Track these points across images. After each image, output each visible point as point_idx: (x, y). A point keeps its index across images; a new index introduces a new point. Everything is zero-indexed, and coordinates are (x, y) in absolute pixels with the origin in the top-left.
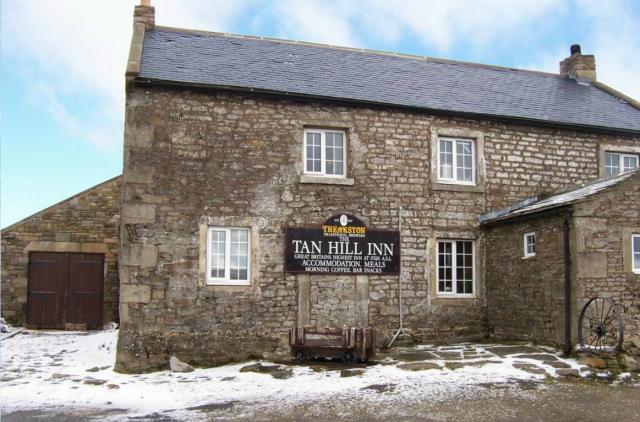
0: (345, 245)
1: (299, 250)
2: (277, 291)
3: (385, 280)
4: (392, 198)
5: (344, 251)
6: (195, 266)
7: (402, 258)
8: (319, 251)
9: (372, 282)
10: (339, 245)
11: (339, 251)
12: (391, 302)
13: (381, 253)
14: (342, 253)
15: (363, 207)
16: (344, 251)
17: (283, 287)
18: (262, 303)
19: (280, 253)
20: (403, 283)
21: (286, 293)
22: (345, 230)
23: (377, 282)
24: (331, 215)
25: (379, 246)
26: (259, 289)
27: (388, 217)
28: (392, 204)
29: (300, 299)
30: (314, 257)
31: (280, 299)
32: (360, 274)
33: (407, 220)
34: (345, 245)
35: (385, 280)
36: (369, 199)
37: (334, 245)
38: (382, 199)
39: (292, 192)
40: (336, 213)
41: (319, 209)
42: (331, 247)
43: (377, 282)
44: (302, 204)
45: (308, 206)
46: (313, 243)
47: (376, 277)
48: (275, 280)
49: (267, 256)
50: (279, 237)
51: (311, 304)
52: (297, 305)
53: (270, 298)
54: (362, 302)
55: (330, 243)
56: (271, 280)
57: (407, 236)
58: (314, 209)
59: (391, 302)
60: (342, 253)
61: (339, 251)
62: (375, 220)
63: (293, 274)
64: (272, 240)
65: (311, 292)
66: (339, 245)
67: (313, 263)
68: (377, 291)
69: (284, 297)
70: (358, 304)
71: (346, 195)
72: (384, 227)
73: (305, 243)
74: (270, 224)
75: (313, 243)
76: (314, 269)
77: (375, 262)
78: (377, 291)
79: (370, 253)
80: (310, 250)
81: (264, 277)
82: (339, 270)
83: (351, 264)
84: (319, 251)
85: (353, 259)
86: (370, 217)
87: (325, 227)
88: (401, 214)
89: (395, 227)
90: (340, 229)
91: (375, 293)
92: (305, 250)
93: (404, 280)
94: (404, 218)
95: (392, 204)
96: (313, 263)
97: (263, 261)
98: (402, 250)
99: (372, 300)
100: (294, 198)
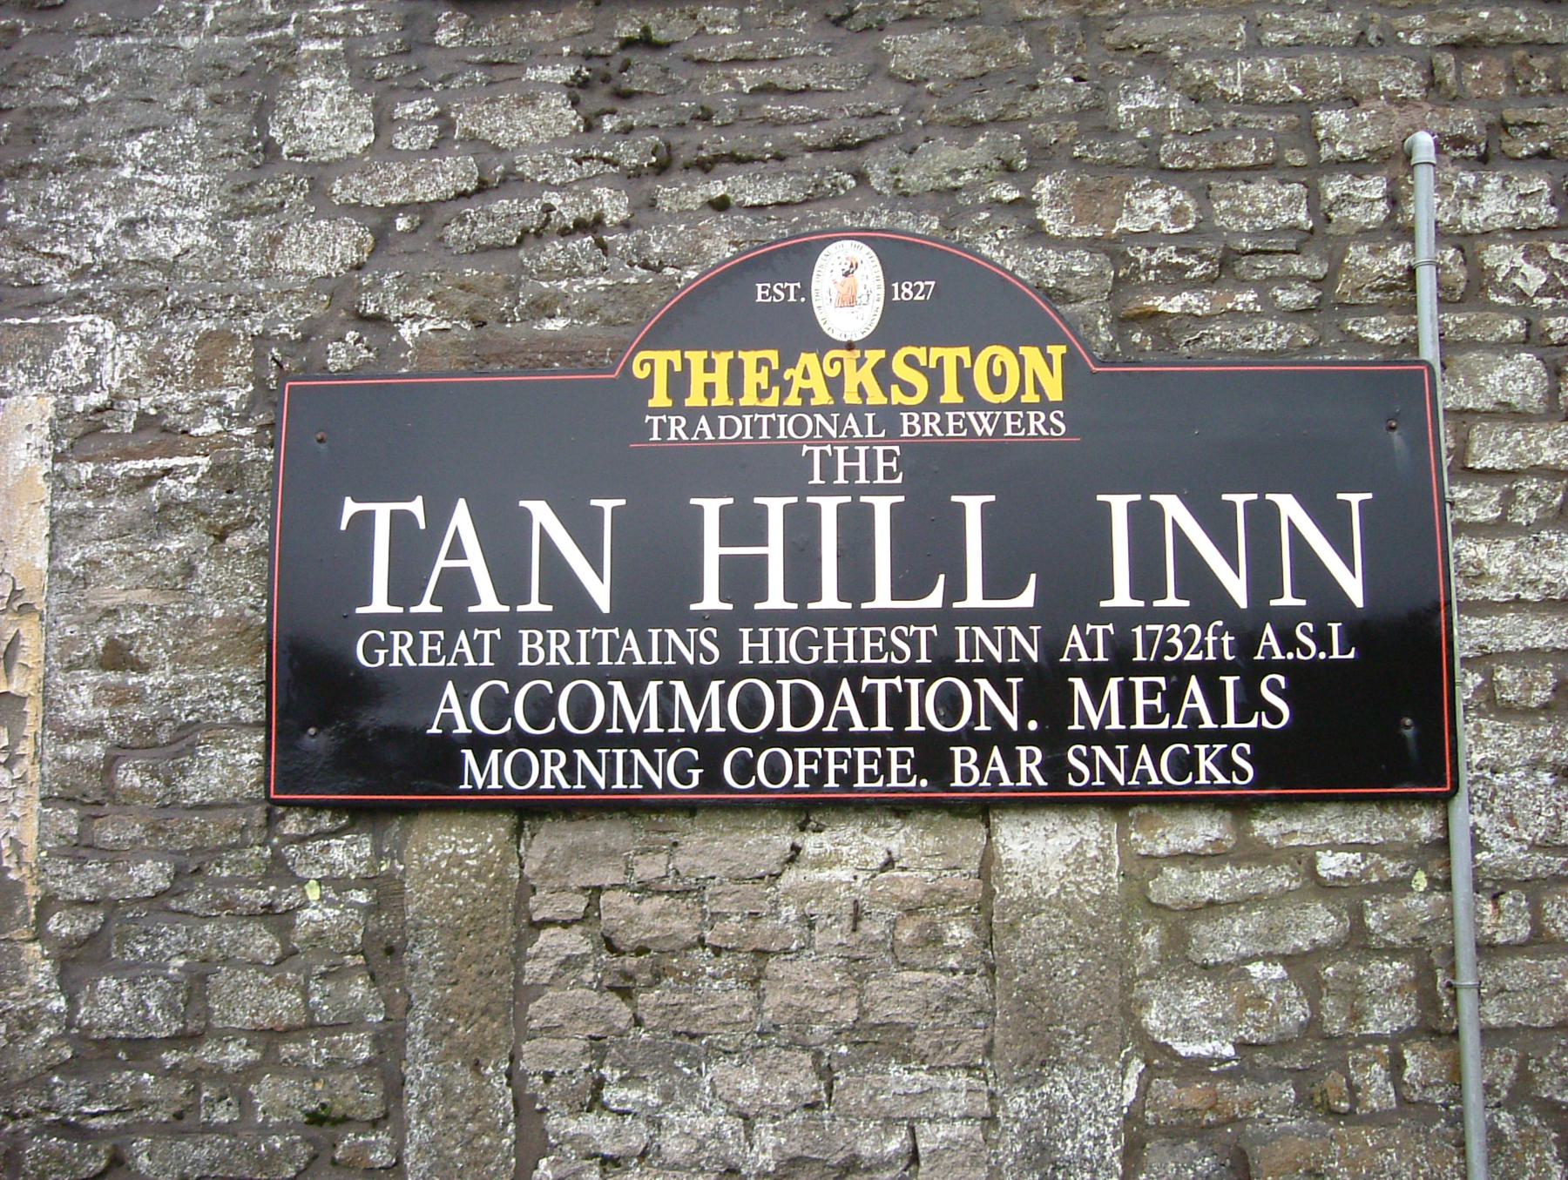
0: (856, 525)
1: (404, 590)
2: (197, 981)
3: (1305, 860)
4: (1334, 68)
5: (856, 580)
6: (1551, 645)
7: (1469, 634)
8: (600, 593)
9: (1173, 885)
10: (802, 525)
11: (803, 580)
12: (1375, 1081)
13: (1237, 588)
14: (830, 599)
15: (1043, 157)
16: (856, 580)
17: (262, 942)
18: (68, 1095)
19: (237, 627)
20: (1492, 885)
21: (285, 1006)
22: (859, 379)
23: (1210, 884)
24: (721, 247)
25: (1219, 527)
26: (39, 967)
27: (1304, 240)
28: (1332, 120)
29: (419, 1073)
30: (555, 648)
31: (237, 1054)
32: (1026, 803)
33: (1502, 258)
34: (856, 525)
35: (1305, 860)
36: (1104, 88)
37: (756, 638)
38: (1233, 80)
39: (363, 79)
40: (776, 229)
41: (612, 204)
42: (746, 645)
43: (1210, 884)
44: (452, 174)
45: (511, 180)
46: (541, 513)
47: (1205, 830)
48: (185, 875)
49: (117, 657)
50: (228, 475)
51: (526, 1111)
52: (389, 1117)
53: (141, 1049)
54: (1059, 1087)
55: (746, 632)
56: (150, 874)
57: (1508, 414)
58: (566, 210)
59: (1375, 1081)
60: (830, 599)
61: (803, 580)
62: (1174, 278)
63: (360, 815)
64: (165, 517)
65: (524, 993)
66: (802, 525)
67: (541, 708)
68: (1227, 973)
69: (269, 1037)
70: (1018, 1102)
71: (877, 69)
72: (1271, 335)
73: (630, 635)
74: (159, 366)
75: (541, 513)
76: (549, 770)
77: (1180, 673)
78: (1227, 973)
79: (1122, 597)
80: (510, 585)
81: (79, 850)
82: (797, 768)
83: (924, 709)
84: (600, 593)
85: (943, 663)
86: (1112, 248)
87: (657, 364)
88: (1426, 207)
89: (1378, 330)
90: (810, 371)
91: (1196, 999)
92: (458, 587)
93: (1505, 851)
94: (1465, 242)
95: (1332, 120)
96: (541, 708)
97: (81, 704)
98: (1467, 550)
99: (1159, 1059)
100: (384, 123)
